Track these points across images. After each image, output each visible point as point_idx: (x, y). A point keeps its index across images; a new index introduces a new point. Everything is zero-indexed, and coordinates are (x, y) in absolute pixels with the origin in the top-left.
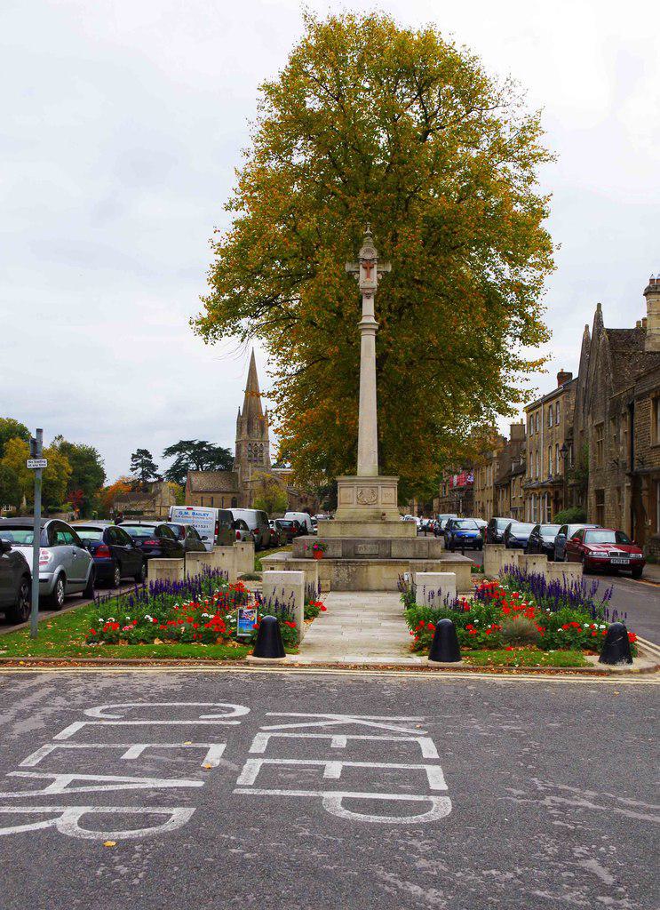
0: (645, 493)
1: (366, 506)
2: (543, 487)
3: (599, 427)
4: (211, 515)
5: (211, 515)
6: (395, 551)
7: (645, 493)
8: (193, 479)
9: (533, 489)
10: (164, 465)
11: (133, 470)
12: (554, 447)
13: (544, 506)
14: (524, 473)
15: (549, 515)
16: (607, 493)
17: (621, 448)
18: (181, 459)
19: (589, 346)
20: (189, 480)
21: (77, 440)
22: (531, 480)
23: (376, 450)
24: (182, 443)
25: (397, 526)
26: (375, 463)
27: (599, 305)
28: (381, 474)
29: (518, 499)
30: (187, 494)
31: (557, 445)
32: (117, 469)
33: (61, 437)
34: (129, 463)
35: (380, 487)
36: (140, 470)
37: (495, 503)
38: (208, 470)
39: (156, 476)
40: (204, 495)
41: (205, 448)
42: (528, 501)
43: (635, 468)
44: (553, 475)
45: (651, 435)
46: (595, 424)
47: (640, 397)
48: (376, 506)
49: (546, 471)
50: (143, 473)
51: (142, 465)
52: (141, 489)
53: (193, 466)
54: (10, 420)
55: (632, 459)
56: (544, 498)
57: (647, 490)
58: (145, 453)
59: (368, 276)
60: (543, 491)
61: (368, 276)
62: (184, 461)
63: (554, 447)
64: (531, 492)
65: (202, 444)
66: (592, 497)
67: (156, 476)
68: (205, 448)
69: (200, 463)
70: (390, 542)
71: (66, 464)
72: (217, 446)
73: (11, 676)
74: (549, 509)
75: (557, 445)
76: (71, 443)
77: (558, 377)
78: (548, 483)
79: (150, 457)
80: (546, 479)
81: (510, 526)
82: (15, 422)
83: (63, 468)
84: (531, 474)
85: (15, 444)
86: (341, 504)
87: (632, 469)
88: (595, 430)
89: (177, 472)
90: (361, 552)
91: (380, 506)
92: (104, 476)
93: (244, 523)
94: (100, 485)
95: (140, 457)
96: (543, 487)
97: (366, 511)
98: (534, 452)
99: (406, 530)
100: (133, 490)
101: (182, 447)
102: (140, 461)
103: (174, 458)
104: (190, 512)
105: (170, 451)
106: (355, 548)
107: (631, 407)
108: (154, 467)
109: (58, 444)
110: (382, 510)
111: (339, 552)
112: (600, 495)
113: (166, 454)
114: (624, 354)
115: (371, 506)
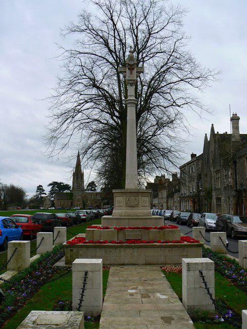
7: (244, 198)
14: (179, 191)
16: (223, 198)
17: (230, 180)
19: (207, 144)
27: (206, 134)
32: (30, 194)
37: (167, 202)
42: (182, 203)
43: (238, 188)
52: (38, 202)
55: (236, 184)
56: (189, 201)
57: (245, 197)
58: (41, 186)
59: (131, 74)
61: (131, 74)
66: (214, 201)
77: (231, 120)
80: (189, 194)
87: (237, 188)
107: (235, 163)
108: (43, 190)
112: (219, 199)
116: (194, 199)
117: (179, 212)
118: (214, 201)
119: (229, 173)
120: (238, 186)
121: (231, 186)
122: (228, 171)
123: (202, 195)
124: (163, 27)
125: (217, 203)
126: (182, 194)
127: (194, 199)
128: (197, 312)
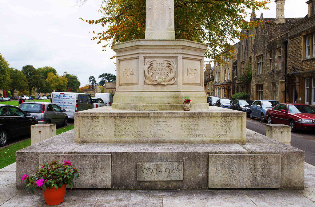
0: (298, 84)
1: (159, 87)
2: (223, 84)
3: (260, 57)
4: (73, 97)
5: (73, 97)
6: (217, 176)
8: (107, 84)
9: (218, 85)
10: (98, 80)
11: (89, 82)
12: (227, 70)
13: (223, 92)
14: (213, 80)
15: (225, 95)
16: (265, 86)
18: (103, 79)
20: (105, 85)
21: (71, 73)
22: (216, 82)
23: (172, 7)
24: (104, 74)
25: (213, 121)
26: (171, 24)
28: (178, 36)
29: (210, 90)
30: (105, 89)
31: (229, 69)
33: (66, 72)
34: (88, 80)
35: (180, 57)
36: (91, 82)
38: (111, 82)
39: (96, 84)
40: (110, 89)
41: (110, 76)
42: (215, 90)
44: (227, 80)
45: (302, 55)
46: (256, 55)
47: (292, 37)
48: (173, 88)
49: (223, 79)
50: (92, 83)
51: (92, 81)
53: (107, 81)
54: (50, 67)
57: (299, 82)
58: (93, 77)
60: (223, 86)
62: (104, 80)
63: (227, 70)
64: (217, 86)
65: (109, 74)
67: (96, 84)
68: (110, 76)
69: (109, 80)
70: (207, 156)
71: (66, 80)
72: (114, 75)
73: (275, 39)
74: (225, 93)
75: (229, 69)
76: (41, 67)
78: (225, 83)
79: (94, 78)
81: (219, 100)
82: (52, 68)
83: (65, 81)
84: (216, 80)
85: (50, 74)
86: (120, 85)
88: (256, 59)
89: (102, 83)
90: (150, 177)
91: (181, 87)
92: (79, 84)
93: (101, 100)
94: (78, 87)
95: (91, 78)
96: (223, 84)
97: (160, 96)
98: (218, 73)
99: (228, 129)
100: (89, 88)
101: (103, 75)
102: (91, 79)
103: (101, 78)
104: (62, 95)
105: (100, 76)
106: (138, 169)
107: (286, 43)
108: (95, 81)
109: (65, 74)
110: (183, 95)
111: (105, 177)
113: (99, 77)
114: (271, 25)
115: (165, 89)
116: (228, 87)
117: (217, 98)
118: (65, 104)
119: (276, 57)
120: (288, 70)
121: (279, 72)
122: (274, 54)
123: (237, 82)
124: (9, 170)
125: (257, 90)
126: (216, 82)
127: (228, 87)
128: (199, 182)
